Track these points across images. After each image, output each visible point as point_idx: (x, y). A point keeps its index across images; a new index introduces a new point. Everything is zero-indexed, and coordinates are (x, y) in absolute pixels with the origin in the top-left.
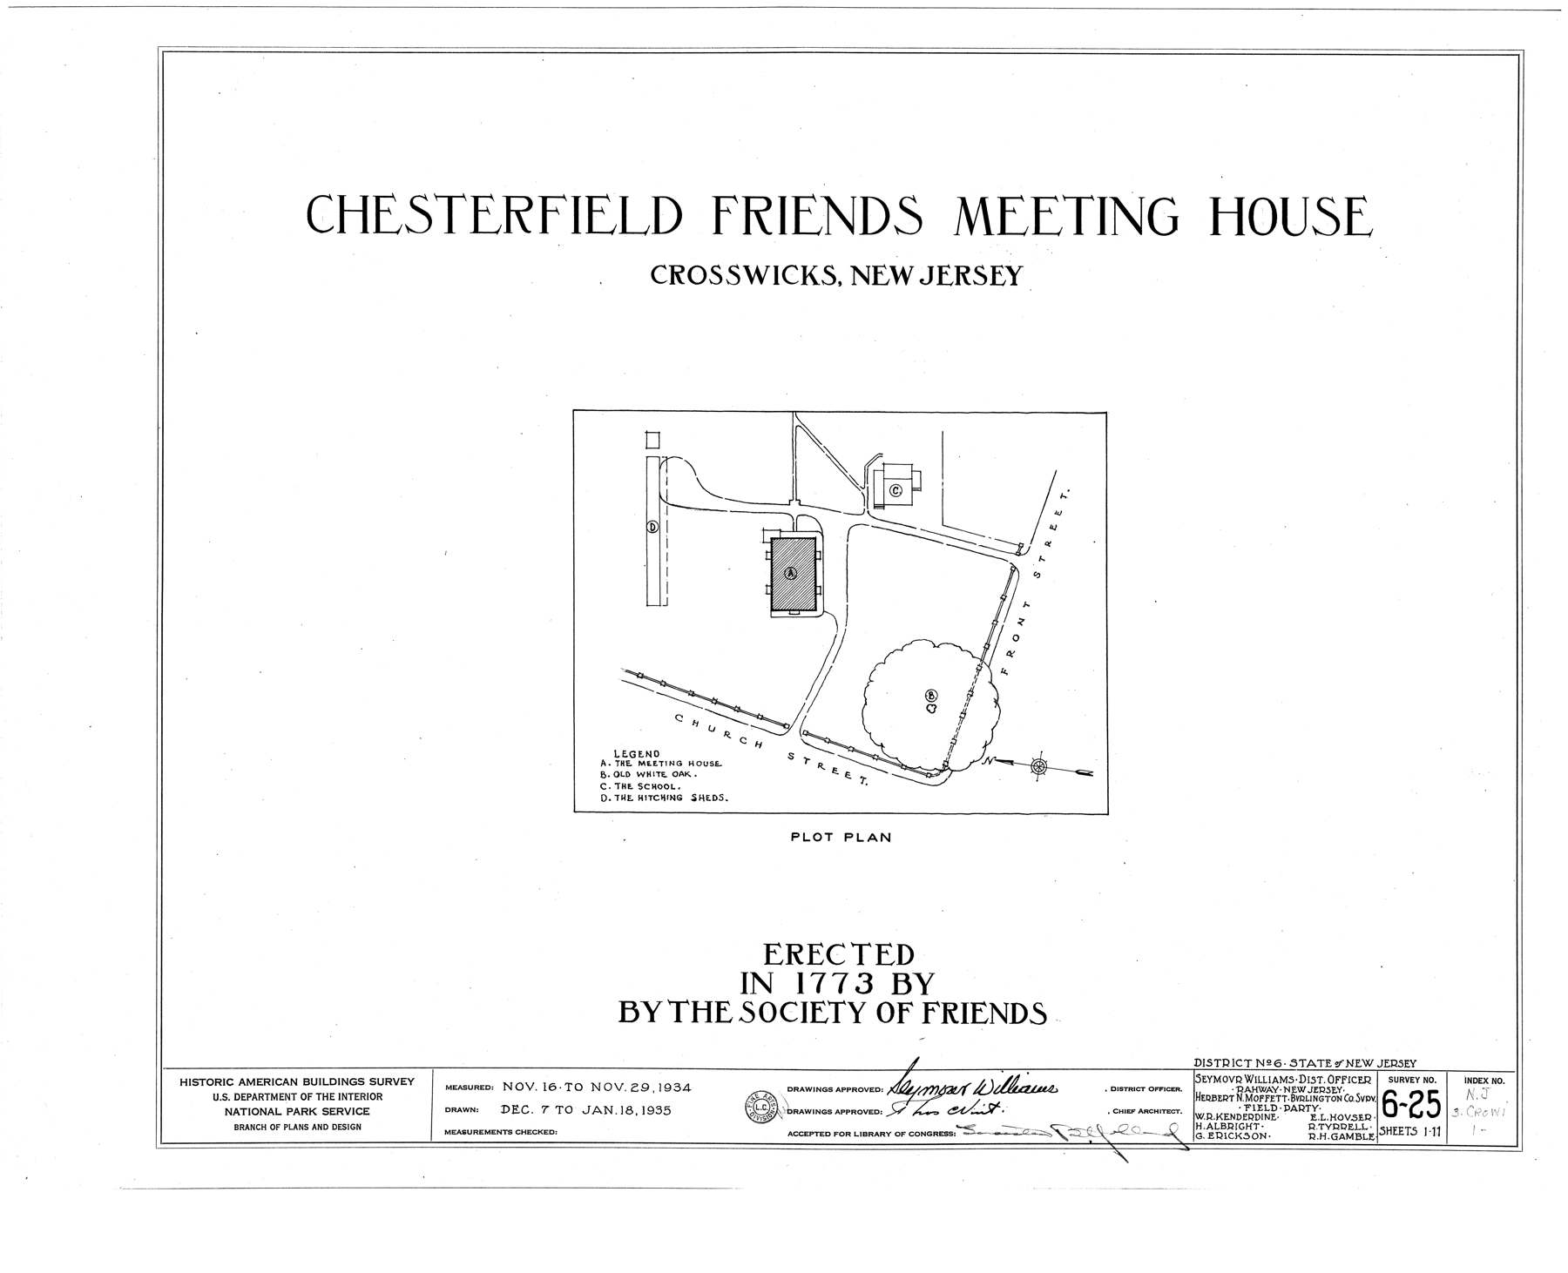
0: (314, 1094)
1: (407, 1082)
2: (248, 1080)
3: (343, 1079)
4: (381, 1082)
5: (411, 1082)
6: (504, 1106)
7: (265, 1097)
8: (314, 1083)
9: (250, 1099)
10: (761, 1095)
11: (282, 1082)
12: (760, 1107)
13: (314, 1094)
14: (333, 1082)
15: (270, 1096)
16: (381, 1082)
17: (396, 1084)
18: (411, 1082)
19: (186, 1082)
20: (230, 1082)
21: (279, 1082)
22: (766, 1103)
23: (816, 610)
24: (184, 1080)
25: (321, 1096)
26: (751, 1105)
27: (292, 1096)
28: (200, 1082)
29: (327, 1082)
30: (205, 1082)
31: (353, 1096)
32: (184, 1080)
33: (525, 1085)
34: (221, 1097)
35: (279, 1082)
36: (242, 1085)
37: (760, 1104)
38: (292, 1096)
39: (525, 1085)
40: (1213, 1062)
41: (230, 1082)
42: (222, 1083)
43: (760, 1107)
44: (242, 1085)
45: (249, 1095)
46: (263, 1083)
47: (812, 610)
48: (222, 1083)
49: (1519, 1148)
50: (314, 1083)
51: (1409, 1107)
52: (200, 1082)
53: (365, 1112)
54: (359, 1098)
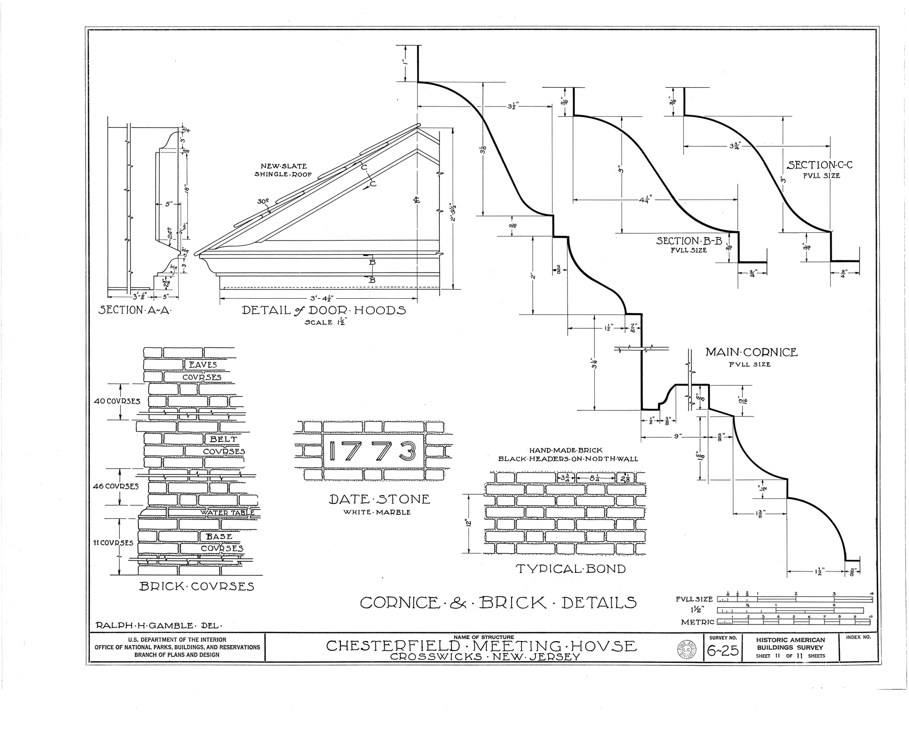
0: (187, 638)
1: (819, 648)
2: (821, 639)
3: (780, 646)
4: (804, 648)
5: (821, 648)
6: (97, 623)
7: (159, 640)
8: (764, 648)
9: (150, 641)
10: (687, 643)
11: (816, 640)
12: (686, 649)
13: (187, 638)
14: (775, 647)
15: (161, 639)
16: (804, 648)
17: (813, 649)
18: (821, 648)
19: (760, 640)
20: (786, 640)
21: (814, 640)
22: (689, 647)
23: (878, 662)
24: (759, 639)
25: (191, 639)
26: (681, 648)
27: (174, 640)
28: (768, 640)
29: (771, 647)
30: (771, 640)
31: (209, 639)
32: (759, 639)
33: (209, 585)
34: (133, 640)
35: (814, 640)
36: (793, 642)
37: (686, 648)
38: (174, 640)
39: (209, 585)
40: (369, 643)
41: (786, 640)
42: (809, 641)
43: (686, 649)
44: (793, 642)
45: (149, 639)
46: (805, 640)
47: (877, 662)
48: (781, 641)
49: (880, 663)
50: (764, 648)
51: (373, 605)
52: (768, 640)
53: (758, 656)
54: (213, 640)
